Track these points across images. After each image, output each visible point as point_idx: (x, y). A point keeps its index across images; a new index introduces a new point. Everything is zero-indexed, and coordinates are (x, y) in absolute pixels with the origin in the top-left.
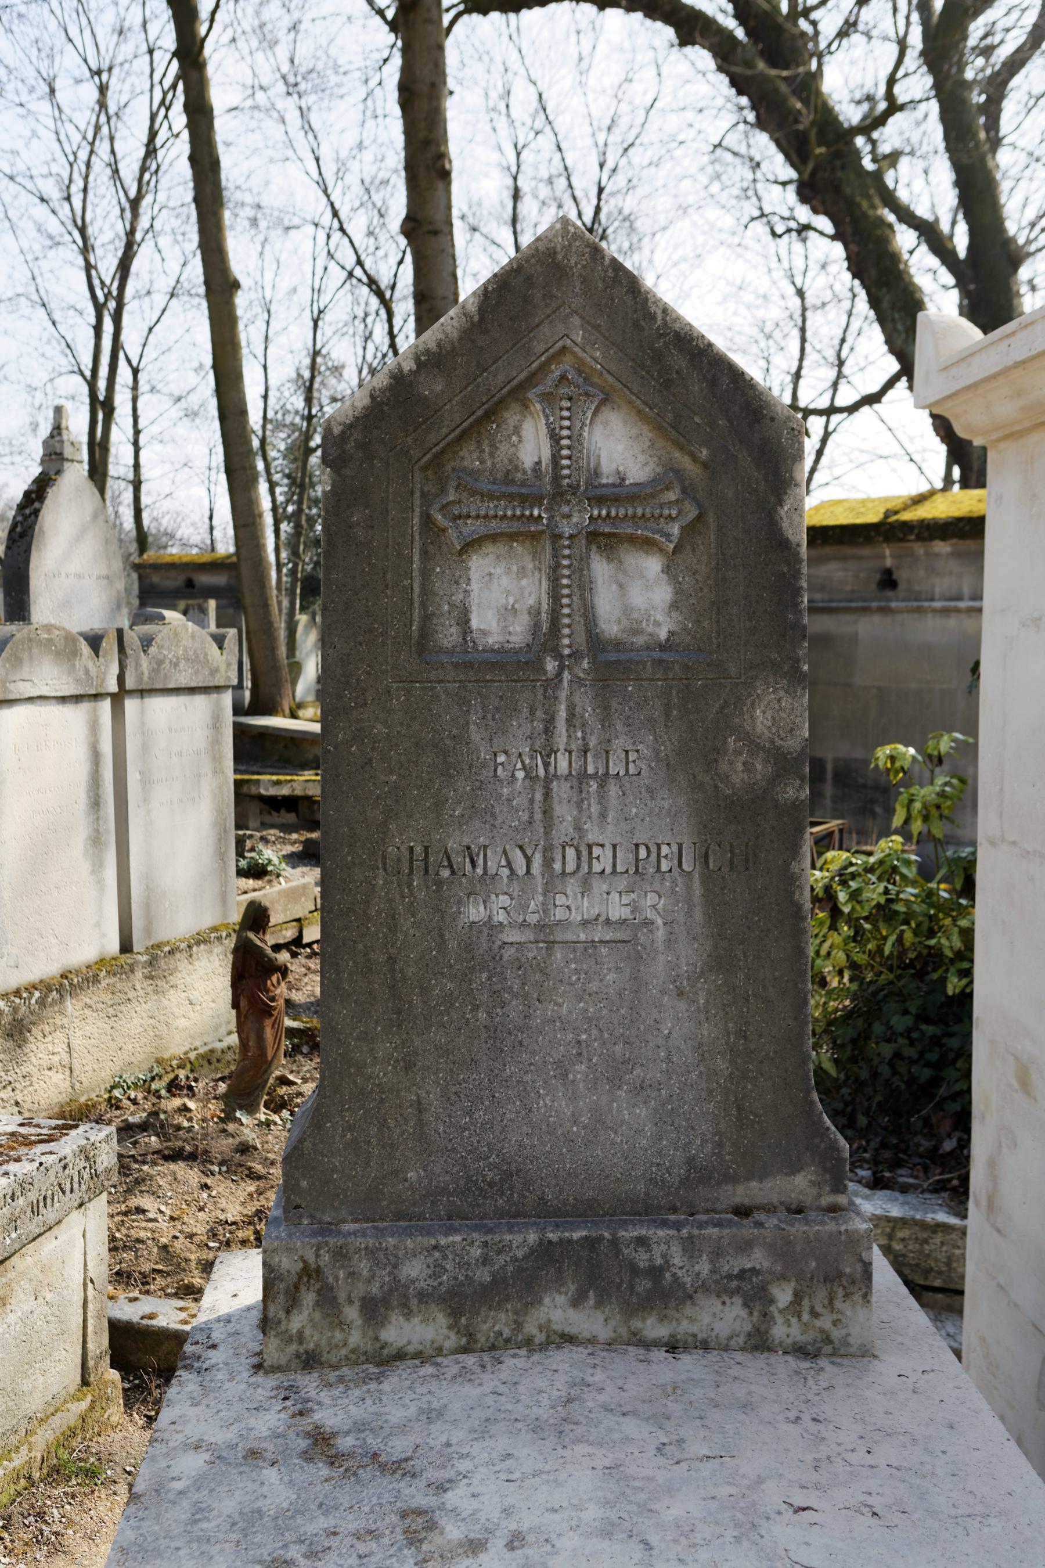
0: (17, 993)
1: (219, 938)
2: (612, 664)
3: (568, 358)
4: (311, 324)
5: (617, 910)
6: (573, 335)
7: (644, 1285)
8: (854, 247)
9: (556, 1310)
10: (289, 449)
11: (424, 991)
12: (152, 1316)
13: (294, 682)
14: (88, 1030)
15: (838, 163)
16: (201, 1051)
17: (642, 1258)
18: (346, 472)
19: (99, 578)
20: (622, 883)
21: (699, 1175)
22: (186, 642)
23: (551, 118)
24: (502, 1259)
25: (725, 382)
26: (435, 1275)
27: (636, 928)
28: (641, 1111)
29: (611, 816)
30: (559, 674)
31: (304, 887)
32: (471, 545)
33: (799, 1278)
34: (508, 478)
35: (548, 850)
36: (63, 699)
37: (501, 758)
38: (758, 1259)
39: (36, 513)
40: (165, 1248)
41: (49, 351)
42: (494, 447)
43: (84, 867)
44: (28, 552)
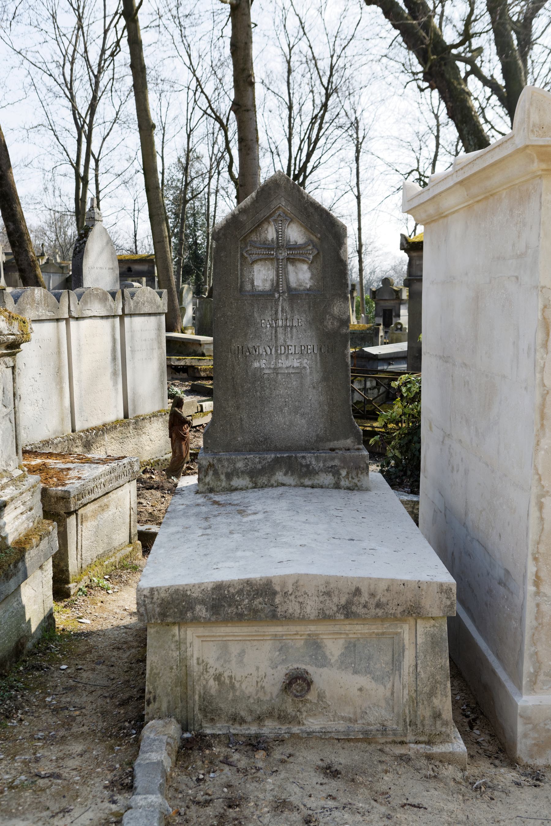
0: (87, 430)
1: (161, 415)
2: (294, 295)
3: (281, 209)
4: (186, 136)
5: (296, 364)
6: (282, 203)
7: (304, 470)
8: (450, 104)
9: (280, 476)
10: (175, 199)
11: (242, 387)
12: (149, 529)
13: (182, 317)
14: (113, 447)
15: (443, 63)
16: (155, 459)
17: (304, 462)
18: (220, 242)
19: (109, 269)
20: (297, 356)
21: (320, 439)
22: (147, 295)
23: (306, 31)
24: (264, 462)
25: (325, 216)
26: (246, 466)
27: (301, 369)
28: (303, 421)
29: (294, 337)
30: (279, 298)
31: (193, 402)
32: (254, 262)
33: (348, 468)
34: (264, 243)
35: (276, 347)
36: (102, 317)
37: (263, 321)
38: (336, 462)
39: (85, 242)
40: (151, 513)
41: (55, 152)
42: (260, 234)
43: (110, 383)
44: (82, 258)
